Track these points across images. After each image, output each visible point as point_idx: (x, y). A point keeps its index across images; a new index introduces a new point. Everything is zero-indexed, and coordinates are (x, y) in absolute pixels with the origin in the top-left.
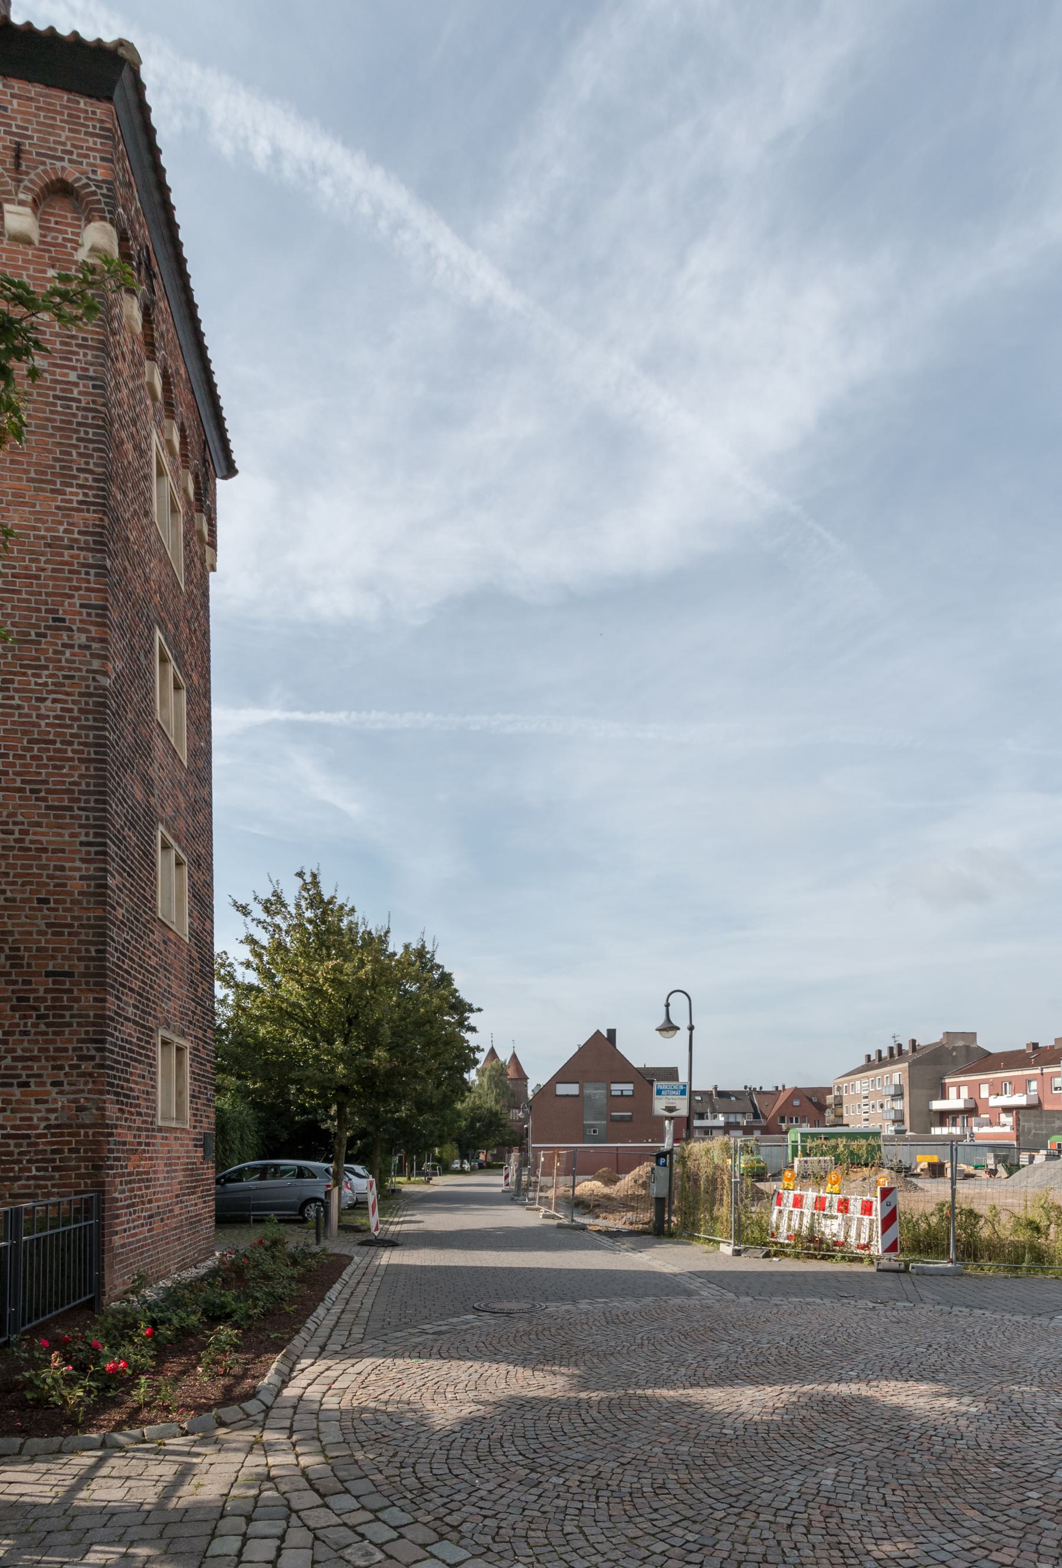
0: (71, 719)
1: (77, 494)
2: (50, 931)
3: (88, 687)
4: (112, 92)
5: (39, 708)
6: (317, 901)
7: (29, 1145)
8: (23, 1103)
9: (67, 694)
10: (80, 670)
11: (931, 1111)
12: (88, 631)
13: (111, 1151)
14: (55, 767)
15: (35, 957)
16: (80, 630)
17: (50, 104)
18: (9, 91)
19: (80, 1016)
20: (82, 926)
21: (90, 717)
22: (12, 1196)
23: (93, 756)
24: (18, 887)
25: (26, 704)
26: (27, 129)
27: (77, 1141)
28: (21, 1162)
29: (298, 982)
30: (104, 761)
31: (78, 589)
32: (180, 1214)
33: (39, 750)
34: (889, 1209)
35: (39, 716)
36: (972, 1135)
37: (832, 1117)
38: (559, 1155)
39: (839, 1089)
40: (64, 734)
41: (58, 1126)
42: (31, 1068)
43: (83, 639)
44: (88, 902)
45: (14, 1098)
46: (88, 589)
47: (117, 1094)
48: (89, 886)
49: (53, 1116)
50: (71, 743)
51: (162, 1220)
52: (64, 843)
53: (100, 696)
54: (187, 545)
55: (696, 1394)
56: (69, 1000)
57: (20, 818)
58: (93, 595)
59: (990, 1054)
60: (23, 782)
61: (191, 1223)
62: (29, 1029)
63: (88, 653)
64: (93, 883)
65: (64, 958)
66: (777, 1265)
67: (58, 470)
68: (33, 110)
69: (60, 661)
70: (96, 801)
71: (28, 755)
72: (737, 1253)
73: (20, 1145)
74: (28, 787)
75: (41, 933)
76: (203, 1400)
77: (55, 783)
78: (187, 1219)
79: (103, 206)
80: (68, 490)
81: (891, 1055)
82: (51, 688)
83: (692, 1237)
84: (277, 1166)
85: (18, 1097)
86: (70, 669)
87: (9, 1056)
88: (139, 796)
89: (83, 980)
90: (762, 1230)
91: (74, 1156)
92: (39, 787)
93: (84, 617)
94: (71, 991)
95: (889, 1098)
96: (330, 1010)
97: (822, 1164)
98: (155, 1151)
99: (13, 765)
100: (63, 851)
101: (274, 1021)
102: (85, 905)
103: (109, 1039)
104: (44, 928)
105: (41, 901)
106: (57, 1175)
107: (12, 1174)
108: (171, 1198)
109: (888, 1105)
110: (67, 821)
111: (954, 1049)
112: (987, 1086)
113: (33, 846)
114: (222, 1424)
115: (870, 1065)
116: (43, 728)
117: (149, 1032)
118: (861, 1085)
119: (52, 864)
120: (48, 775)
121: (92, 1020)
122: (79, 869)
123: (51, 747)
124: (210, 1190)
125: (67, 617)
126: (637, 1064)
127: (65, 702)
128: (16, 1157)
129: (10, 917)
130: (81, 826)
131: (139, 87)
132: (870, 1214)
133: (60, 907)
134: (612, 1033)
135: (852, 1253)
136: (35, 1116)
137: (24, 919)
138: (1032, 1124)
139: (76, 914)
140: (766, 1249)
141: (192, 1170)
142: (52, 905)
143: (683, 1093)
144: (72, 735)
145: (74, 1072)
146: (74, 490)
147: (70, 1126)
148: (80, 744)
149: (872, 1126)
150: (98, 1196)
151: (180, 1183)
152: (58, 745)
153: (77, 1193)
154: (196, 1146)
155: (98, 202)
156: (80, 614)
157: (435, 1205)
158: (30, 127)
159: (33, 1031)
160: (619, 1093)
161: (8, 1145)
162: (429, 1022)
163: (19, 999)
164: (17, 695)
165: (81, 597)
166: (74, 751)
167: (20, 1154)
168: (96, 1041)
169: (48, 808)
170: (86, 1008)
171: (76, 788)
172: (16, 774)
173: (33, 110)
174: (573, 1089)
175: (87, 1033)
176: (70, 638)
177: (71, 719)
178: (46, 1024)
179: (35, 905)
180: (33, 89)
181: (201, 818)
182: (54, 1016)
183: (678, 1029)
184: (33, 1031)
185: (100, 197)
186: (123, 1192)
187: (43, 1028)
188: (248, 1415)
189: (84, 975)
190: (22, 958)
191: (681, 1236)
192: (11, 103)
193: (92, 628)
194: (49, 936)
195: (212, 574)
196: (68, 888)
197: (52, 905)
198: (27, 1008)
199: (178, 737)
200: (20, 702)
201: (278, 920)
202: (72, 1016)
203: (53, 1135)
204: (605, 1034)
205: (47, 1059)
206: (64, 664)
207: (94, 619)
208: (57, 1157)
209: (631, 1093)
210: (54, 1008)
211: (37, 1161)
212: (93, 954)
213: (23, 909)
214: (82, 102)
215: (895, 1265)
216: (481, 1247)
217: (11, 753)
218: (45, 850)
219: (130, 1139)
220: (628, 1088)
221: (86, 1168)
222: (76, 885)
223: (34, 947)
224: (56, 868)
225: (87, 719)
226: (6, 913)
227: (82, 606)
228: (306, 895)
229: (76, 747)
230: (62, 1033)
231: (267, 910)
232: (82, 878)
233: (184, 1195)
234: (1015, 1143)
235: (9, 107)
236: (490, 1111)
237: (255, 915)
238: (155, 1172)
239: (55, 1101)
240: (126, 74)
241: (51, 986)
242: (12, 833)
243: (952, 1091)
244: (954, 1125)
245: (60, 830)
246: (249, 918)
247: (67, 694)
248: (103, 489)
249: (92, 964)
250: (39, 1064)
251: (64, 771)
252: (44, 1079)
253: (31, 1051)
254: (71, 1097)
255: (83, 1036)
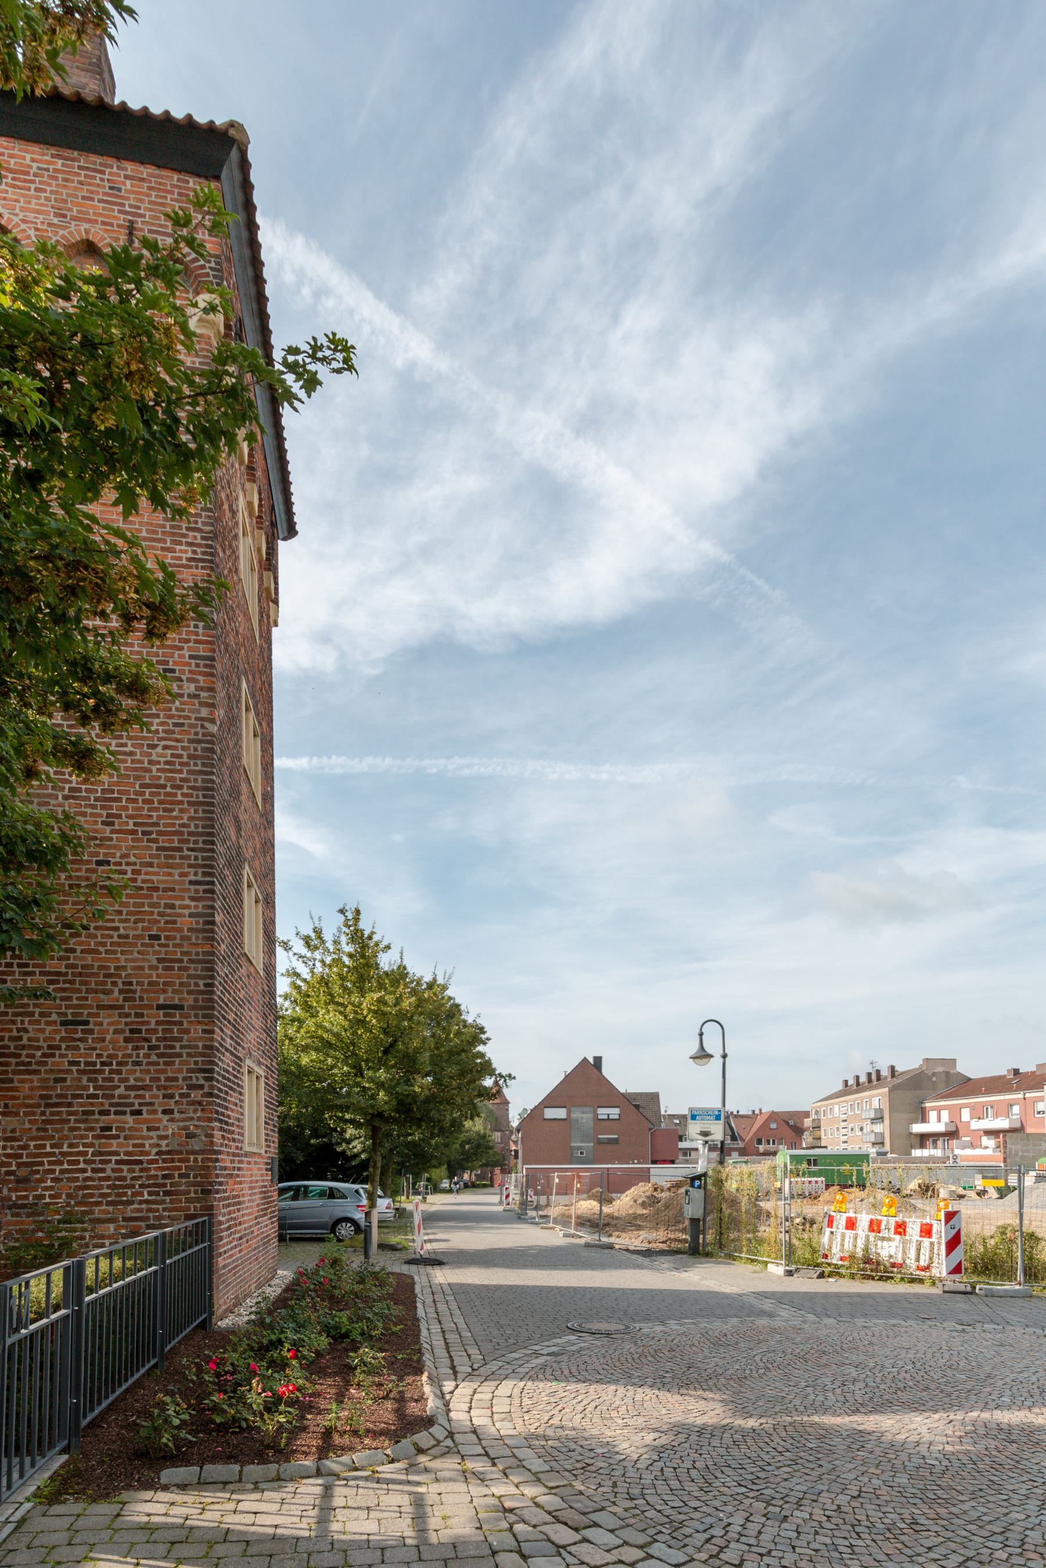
0: (181, 764)
1: (186, 552)
2: (161, 966)
3: (196, 734)
4: (221, 172)
5: (150, 754)
6: (358, 937)
7: (141, 1170)
8: (136, 1130)
9: (177, 740)
10: (189, 718)
11: (911, 1134)
12: (197, 681)
13: (217, 1176)
14: (165, 810)
15: (146, 991)
16: (189, 680)
17: (160, 184)
18: (122, 173)
19: (190, 1047)
20: (191, 961)
21: (199, 762)
22: (125, 1219)
23: (201, 799)
24: (131, 924)
25: (138, 751)
26: (139, 208)
27: (186, 1167)
28: (133, 1186)
29: (341, 1013)
30: (212, 804)
31: (187, 641)
32: (258, 1235)
33: (151, 794)
34: (954, 1232)
35: (150, 762)
36: (955, 1157)
37: (810, 1139)
38: (579, 1177)
39: (817, 1112)
40: (174, 779)
41: (169, 1152)
42: (143, 1097)
43: (192, 688)
44: (197, 938)
45: (127, 1126)
46: (196, 642)
47: (221, 1121)
48: (197, 923)
49: (164, 1143)
50: (180, 787)
51: (247, 1241)
52: (174, 882)
53: (208, 742)
54: (259, 601)
55: (869, 1422)
56: (180, 1031)
57: (132, 859)
58: (201, 646)
59: (970, 1079)
60: (135, 824)
61: (264, 1244)
62: (141, 1059)
63: (196, 702)
64: (201, 920)
65: (174, 992)
66: (832, 1285)
67: (168, 529)
68: (145, 190)
69: (170, 710)
70: (204, 842)
71: (140, 799)
72: (789, 1273)
73: (133, 1171)
74: (140, 829)
75: (151, 968)
76: (383, 1425)
77: (166, 825)
78: (262, 1240)
79: (211, 278)
80: (178, 547)
81: (870, 1081)
82: (161, 735)
83: (731, 1257)
84: (306, 1187)
85: (131, 1124)
86: (180, 717)
87: (122, 1085)
88: (234, 838)
89: (193, 1012)
90: (814, 1251)
91: (184, 1180)
92: (151, 829)
93: (193, 667)
94: (181, 1023)
95: (869, 1122)
96: (370, 1040)
97: (813, 1184)
98: (243, 1176)
99: (126, 809)
100: (173, 890)
101: (317, 1050)
102: (194, 941)
103: (217, 1069)
104: (155, 963)
105: (152, 937)
106: (168, 1199)
107: (125, 1199)
108: (252, 1220)
109: (867, 1128)
110: (177, 861)
111: (934, 1074)
112: (968, 1110)
113: (145, 885)
114: (420, 1451)
115: (847, 1089)
116: (154, 773)
117: (239, 1060)
118: (839, 1109)
119: (163, 902)
120: (159, 817)
121: (200, 1050)
122: (188, 907)
123: (162, 791)
124: (274, 1212)
125: (177, 668)
126: (622, 1091)
127: (175, 748)
128: (129, 1182)
129: (123, 953)
130: (190, 866)
131: (245, 166)
132: (930, 1236)
133: (171, 943)
134: (598, 1060)
135: (911, 1274)
136: (147, 1143)
137: (136, 955)
138: (1019, 1147)
139: (185, 949)
140: (819, 1270)
141: (264, 1192)
142: (163, 941)
143: (718, 1118)
144: (181, 780)
145: (184, 1100)
146: (183, 547)
147: (180, 1152)
148: (189, 788)
149: (853, 1148)
150: (210, 1219)
151: (258, 1205)
152: (169, 789)
153: (188, 1217)
154: (267, 1170)
155: (207, 275)
156: (189, 664)
157: (448, 1224)
158: (143, 206)
159: (145, 1061)
160: (606, 1117)
161: (122, 1171)
162: (464, 1051)
163: (132, 1031)
164: (129, 743)
165: (190, 649)
166: (183, 795)
167: (132, 1179)
168: (204, 1071)
169: (158, 849)
170: (195, 1039)
171: (185, 830)
172: (128, 817)
173: (145, 190)
174: (560, 1113)
175: (196, 1063)
176: (180, 687)
177: (181, 764)
178: (158, 1055)
179: (147, 941)
180: (145, 170)
181: (268, 858)
182: (165, 1047)
183: (711, 1056)
184: (145, 1061)
185: (208, 270)
186: (224, 1215)
187: (154, 1058)
188: (439, 1442)
189: (193, 1008)
190: (134, 992)
191: (718, 1256)
192: (124, 184)
193: (201, 678)
194: (160, 971)
195: (274, 630)
196: (178, 925)
197: (163, 941)
198: (139, 1040)
199: (256, 782)
200: (132, 749)
201: (317, 955)
202: (182, 1047)
203: (164, 1161)
204: (592, 1061)
205: (159, 1088)
206: (174, 712)
207: (202, 669)
208: (168, 1181)
209: (617, 1117)
210: (165, 1039)
211: (149, 1186)
212: (202, 987)
213: (136, 945)
214: (191, 181)
215: (961, 1287)
216: (525, 1266)
217: (124, 797)
218: (156, 889)
219: (228, 1164)
220: (614, 1112)
221: (196, 1192)
222: (185, 922)
223: (146, 981)
224: (167, 906)
225: (196, 765)
226: (119, 949)
227: (191, 657)
228: (347, 931)
229: (185, 791)
230: (173, 1063)
231: (308, 944)
232: (191, 915)
233: (260, 1217)
234: (1002, 1165)
235: (123, 188)
236: (478, 1133)
237: (295, 950)
238: (243, 1195)
239: (166, 1128)
240: (234, 154)
241: (162, 1018)
242: (125, 873)
243: (933, 1115)
244: (935, 1147)
245: (170, 870)
246: (291, 953)
247: (177, 740)
248: (210, 546)
249: (201, 997)
250: (150, 1093)
251: (175, 814)
252: (156, 1107)
253: (143, 1080)
254: (181, 1124)
255: (192, 1066)
